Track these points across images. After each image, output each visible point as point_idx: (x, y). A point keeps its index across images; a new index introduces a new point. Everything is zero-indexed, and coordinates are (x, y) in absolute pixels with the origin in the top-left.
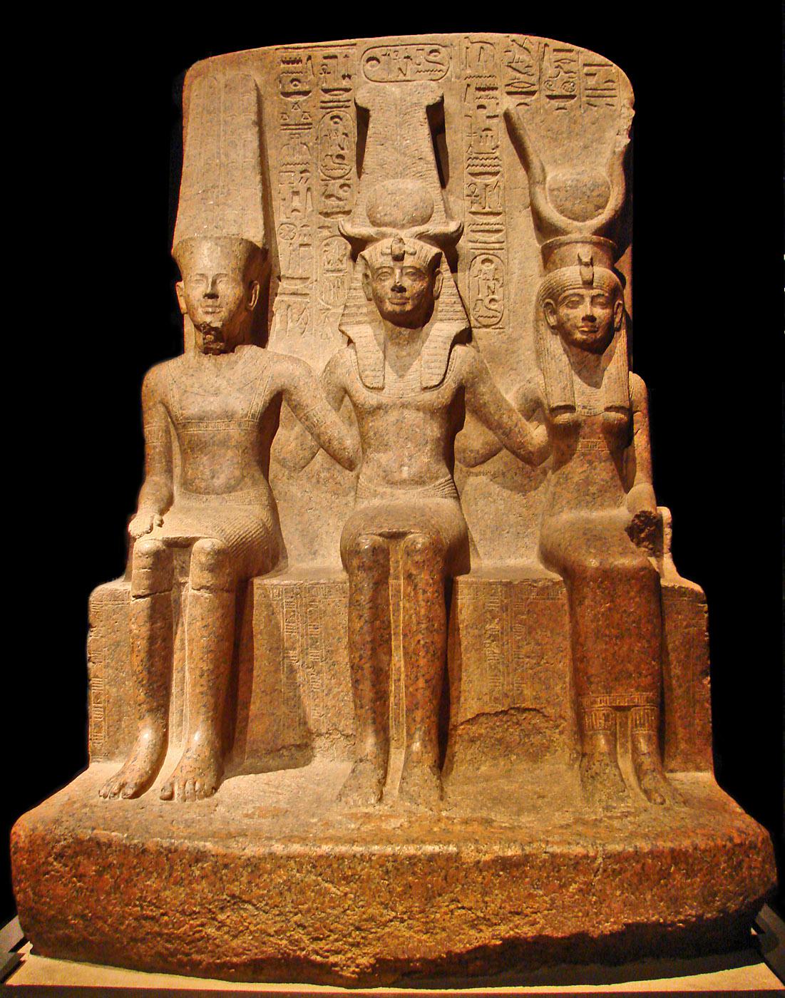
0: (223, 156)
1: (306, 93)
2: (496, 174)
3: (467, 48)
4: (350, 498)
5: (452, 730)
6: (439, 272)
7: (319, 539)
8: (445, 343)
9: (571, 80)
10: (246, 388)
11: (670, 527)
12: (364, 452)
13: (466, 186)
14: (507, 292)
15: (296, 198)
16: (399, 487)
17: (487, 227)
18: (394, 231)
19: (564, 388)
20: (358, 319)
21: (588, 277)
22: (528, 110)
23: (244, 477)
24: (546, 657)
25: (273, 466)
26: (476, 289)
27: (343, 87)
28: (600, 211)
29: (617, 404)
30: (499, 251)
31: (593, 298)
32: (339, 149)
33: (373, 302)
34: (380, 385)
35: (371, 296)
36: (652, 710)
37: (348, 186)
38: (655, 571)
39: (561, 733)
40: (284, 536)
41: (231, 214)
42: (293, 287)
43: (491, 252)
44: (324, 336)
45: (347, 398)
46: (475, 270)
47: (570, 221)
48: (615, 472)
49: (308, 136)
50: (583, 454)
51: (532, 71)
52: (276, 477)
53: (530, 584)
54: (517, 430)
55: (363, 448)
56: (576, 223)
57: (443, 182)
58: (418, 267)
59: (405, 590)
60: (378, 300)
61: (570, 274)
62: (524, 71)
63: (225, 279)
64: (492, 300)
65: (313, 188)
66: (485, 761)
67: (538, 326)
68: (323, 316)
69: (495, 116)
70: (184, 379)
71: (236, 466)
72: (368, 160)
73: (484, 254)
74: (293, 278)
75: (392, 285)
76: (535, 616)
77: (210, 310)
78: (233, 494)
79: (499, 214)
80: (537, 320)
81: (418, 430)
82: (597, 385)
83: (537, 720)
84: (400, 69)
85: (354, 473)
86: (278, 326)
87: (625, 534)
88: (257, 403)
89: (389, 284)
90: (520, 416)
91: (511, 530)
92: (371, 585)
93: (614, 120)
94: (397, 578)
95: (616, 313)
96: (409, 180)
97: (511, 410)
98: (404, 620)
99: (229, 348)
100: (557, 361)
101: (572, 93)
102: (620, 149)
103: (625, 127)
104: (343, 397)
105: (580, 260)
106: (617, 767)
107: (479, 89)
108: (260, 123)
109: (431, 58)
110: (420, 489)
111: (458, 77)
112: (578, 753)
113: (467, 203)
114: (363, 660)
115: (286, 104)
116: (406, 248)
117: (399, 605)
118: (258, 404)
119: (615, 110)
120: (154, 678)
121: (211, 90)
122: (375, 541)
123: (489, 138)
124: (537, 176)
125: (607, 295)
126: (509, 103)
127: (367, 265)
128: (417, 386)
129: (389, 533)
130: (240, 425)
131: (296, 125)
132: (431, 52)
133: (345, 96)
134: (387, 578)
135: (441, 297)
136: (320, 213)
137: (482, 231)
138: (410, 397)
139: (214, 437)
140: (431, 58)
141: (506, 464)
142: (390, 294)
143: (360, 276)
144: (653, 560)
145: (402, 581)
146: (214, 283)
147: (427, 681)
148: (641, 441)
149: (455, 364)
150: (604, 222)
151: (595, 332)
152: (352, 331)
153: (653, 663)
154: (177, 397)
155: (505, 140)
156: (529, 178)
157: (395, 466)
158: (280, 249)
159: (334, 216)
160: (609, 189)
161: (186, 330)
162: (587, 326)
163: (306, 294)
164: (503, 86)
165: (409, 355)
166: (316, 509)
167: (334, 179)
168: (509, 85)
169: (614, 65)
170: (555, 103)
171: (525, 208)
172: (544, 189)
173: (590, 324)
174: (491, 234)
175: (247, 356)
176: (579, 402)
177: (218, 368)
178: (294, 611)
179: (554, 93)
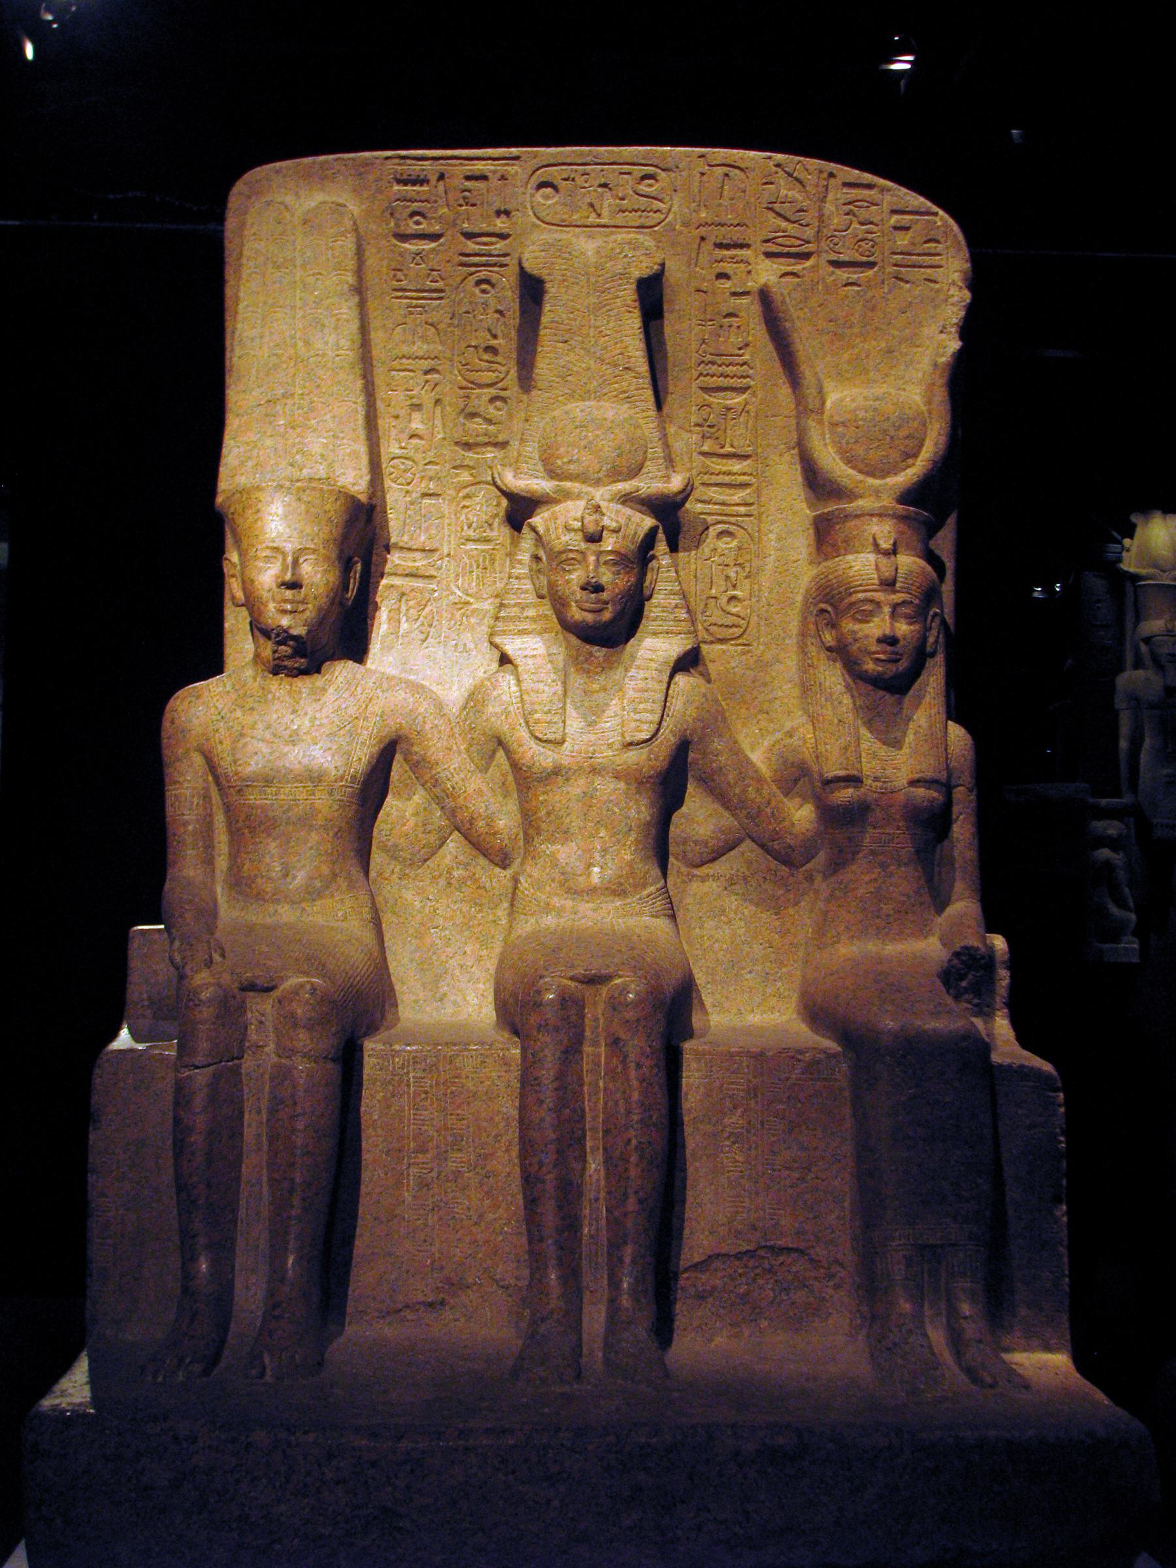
0: (300, 344)
1: (434, 237)
2: (743, 390)
3: (703, 174)
4: (502, 912)
6: (653, 557)
7: (449, 977)
8: (660, 672)
9: (870, 236)
10: (342, 732)
11: (1009, 968)
12: (528, 840)
15: (416, 416)
16: (586, 898)
17: (727, 479)
18: (586, 489)
19: (846, 748)
20: (522, 626)
21: (887, 574)
22: (798, 285)
23: (335, 875)
24: (814, 1169)
25: (377, 858)
26: (707, 580)
27: (497, 230)
28: (910, 461)
29: (929, 775)
31: (895, 607)
32: (489, 337)
33: (546, 601)
34: (558, 737)
35: (545, 592)
37: (504, 400)
38: (983, 1041)
39: (837, 1287)
40: (391, 971)
41: (316, 444)
42: (410, 564)
43: (733, 519)
44: (461, 648)
45: (501, 754)
46: (706, 549)
47: (860, 477)
48: (922, 882)
50: (873, 853)
51: (807, 218)
52: (380, 874)
53: (793, 1055)
55: (526, 834)
56: (871, 481)
57: (659, 405)
58: (623, 551)
59: (607, 1063)
60: (559, 604)
61: (862, 565)
62: (792, 218)
63: (313, 557)
65: (446, 400)
66: (721, 1329)
67: (806, 645)
68: (458, 615)
70: (239, 714)
71: (324, 858)
72: (543, 367)
73: (719, 522)
74: (410, 549)
75: (583, 581)
76: (799, 1105)
77: (289, 607)
78: (318, 903)
79: (747, 457)
80: (803, 634)
81: (616, 810)
82: (897, 744)
83: (800, 1266)
84: (591, 205)
85: (509, 872)
86: (384, 627)
87: (938, 983)
88: (362, 756)
89: (576, 577)
90: (774, 788)
91: (756, 968)
92: (558, 1054)
93: (936, 307)
94: (595, 1044)
95: (930, 628)
96: (607, 404)
97: (760, 780)
98: (605, 1108)
99: (314, 669)
100: (836, 703)
101: (871, 259)
102: (944, 359)
103: (955, 321)
104: (494, 752)
105: (876, 544)
106: (925, 1335)
107: (720, 246)
108: (359, 290)
109: (643, 188)
112: (863, 1317)
113: (695, 438)
114: (544, 1168)
115: (401, 255)
116: (606, 521)
117: (597, 1085)
118: (360, 759)
119: (938, 291)
121: (280, 228)
122: (565, 986)
124: (810, 400)
125: (917, 601)
126: (767, 273)
127: (539, 539)
128: (616, 739)
129: (585, 976)
130: (331, 794)
133: (500, 246)
134: (581, 1044)
135: (655, 596)
136: (457, 443)
137: (717, 485)
138: (605, 755)
139: (288, 810)
141: (749, 863)
142: (579, 594)
143: (525, 557)
144: (978, 1022)
145: (603, 1048)
146: (296, 563)
147: (640, 1202)
148: (963, 831)
149: (677, 704)
150: (915, 479)
151: (897, 661)
152: (512, 646)
154: (227, 744)
155: (758, 332)
156: (798, 404)
157: (580, 866)
159: (478, 450)
160: (924, 425)
161: (227, 625)
162: (884, 653)
163: (432, 577)
164: (759, 243)
165: (604, 689)
166: (444, 929)
167: (480, 386)
168: (767, 241)
169: (941, 213)
170: (843, 275)
171: (789, 449)
172: (821, 422)
173: (888, 648)
174: (732, 491)
175: (340, 679)
176: (868, 767)
177: (294, 695)
178: (426, 1092)
179: (842, 257)
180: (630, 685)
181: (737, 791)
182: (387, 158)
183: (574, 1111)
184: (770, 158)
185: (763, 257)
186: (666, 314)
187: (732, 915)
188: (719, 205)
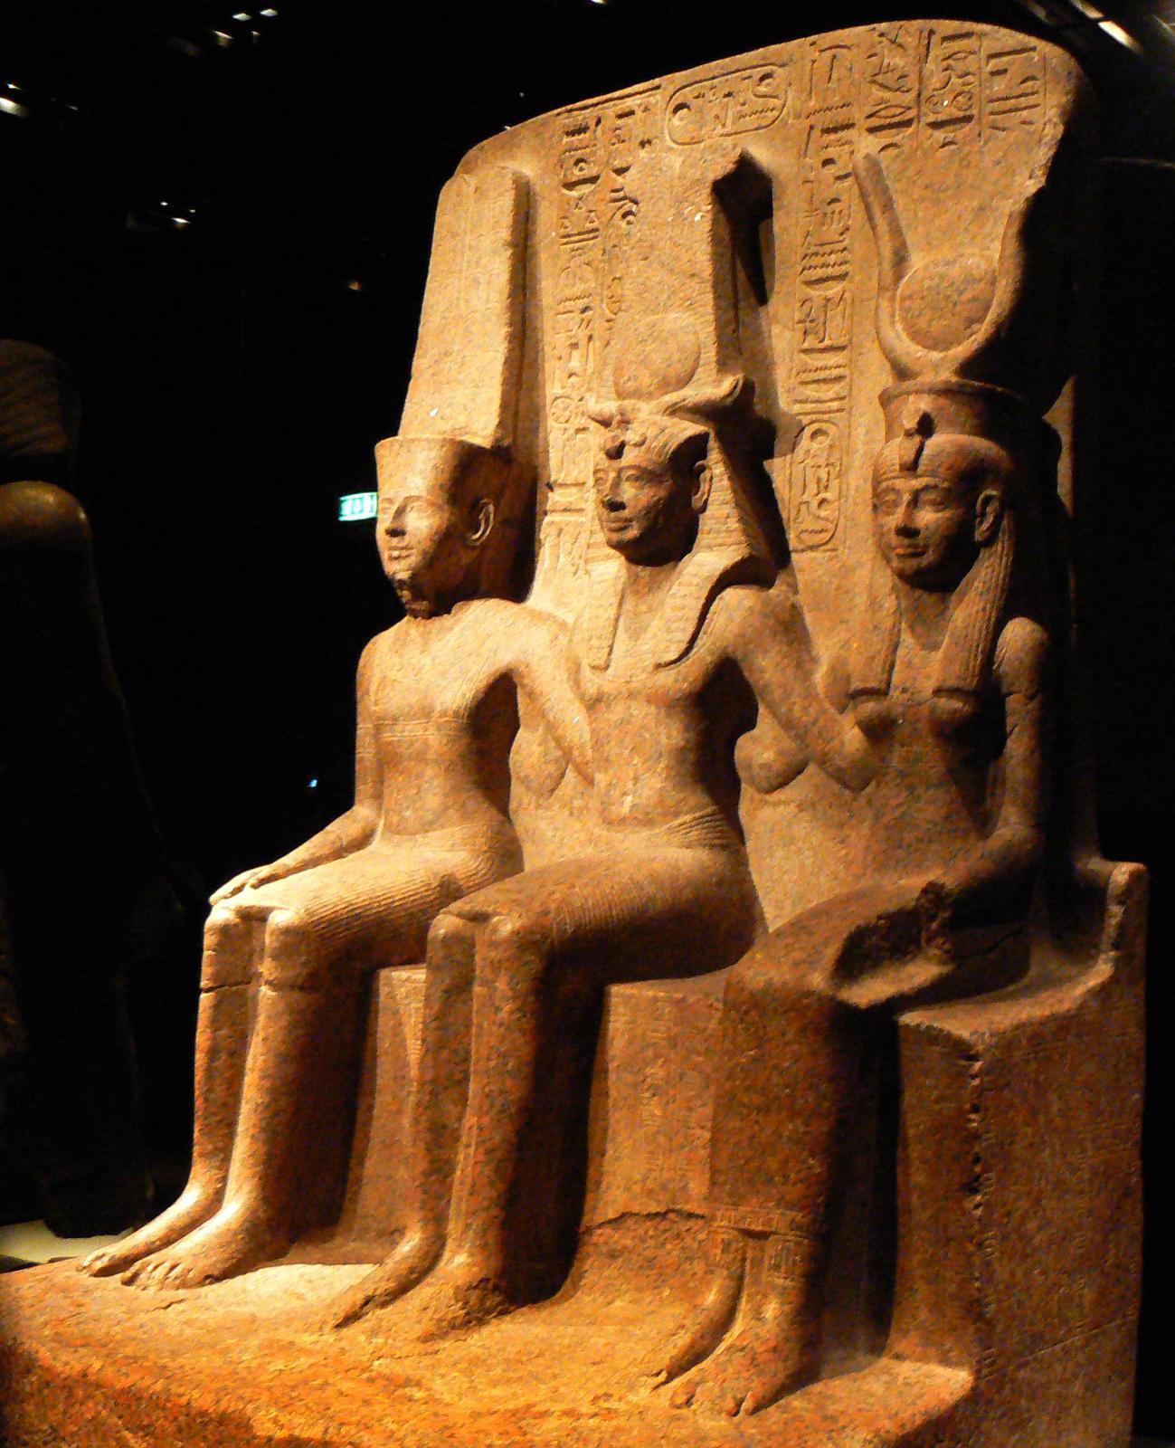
1: (593, 180)
5: (584, 1233)
13: (798, 305)
14: (844, 486)
15: (576, 354)
17: (823, 375)
22: (897, 157)
26: (800, 484)
28: (975, 327)
29: (951, 683)
30: (838, 414)
36: (798, 1244)
43: (826, 417)
46: (800, 451)
49: (594, 249)
50: (902, 774)
52: (520, 804)
54: (815, 730)
58: (644, 464)
64: (822, 502)
65: (595, 337)
69: (847, 176)
78: (429, 834)
79: (843, 348)
81: (648, 736)
101: (968, 113)
107: (827, 131)
109: (762, 89)
110: (645, 833)
111: (798, 116)
120: (213, 1109)
123: (836, 216)
131: (579, 234)
132: (762, 79)
135: (709, 508)
137: (817, 381)
140: (762, 89)
141: (817, 788)
151: (922, 554)
153: (811, 1162)
158: (551, 438)
162: (901, 546)
163: (581, 510)
170: (940, 135)
173: (906, 541)
174: (830, 385)
179: (940, 118)
180: (670, 602)
181: (783, 710)
182: (558, 114)
183: (455, 1052)
184: (874, 29)
185: (866, 134)
186: (774, 212)
187: (800, 844)
188: (828, 89)
